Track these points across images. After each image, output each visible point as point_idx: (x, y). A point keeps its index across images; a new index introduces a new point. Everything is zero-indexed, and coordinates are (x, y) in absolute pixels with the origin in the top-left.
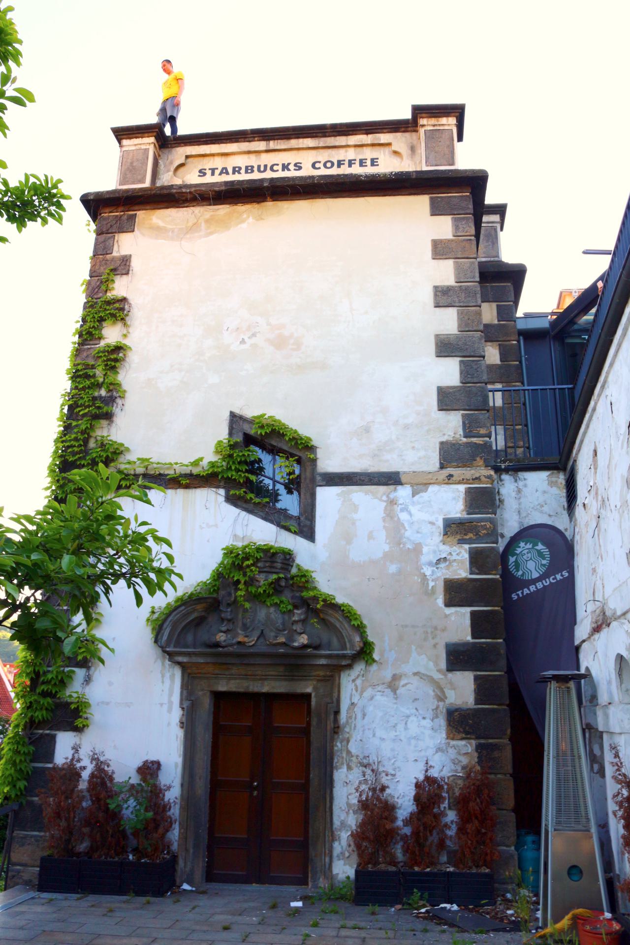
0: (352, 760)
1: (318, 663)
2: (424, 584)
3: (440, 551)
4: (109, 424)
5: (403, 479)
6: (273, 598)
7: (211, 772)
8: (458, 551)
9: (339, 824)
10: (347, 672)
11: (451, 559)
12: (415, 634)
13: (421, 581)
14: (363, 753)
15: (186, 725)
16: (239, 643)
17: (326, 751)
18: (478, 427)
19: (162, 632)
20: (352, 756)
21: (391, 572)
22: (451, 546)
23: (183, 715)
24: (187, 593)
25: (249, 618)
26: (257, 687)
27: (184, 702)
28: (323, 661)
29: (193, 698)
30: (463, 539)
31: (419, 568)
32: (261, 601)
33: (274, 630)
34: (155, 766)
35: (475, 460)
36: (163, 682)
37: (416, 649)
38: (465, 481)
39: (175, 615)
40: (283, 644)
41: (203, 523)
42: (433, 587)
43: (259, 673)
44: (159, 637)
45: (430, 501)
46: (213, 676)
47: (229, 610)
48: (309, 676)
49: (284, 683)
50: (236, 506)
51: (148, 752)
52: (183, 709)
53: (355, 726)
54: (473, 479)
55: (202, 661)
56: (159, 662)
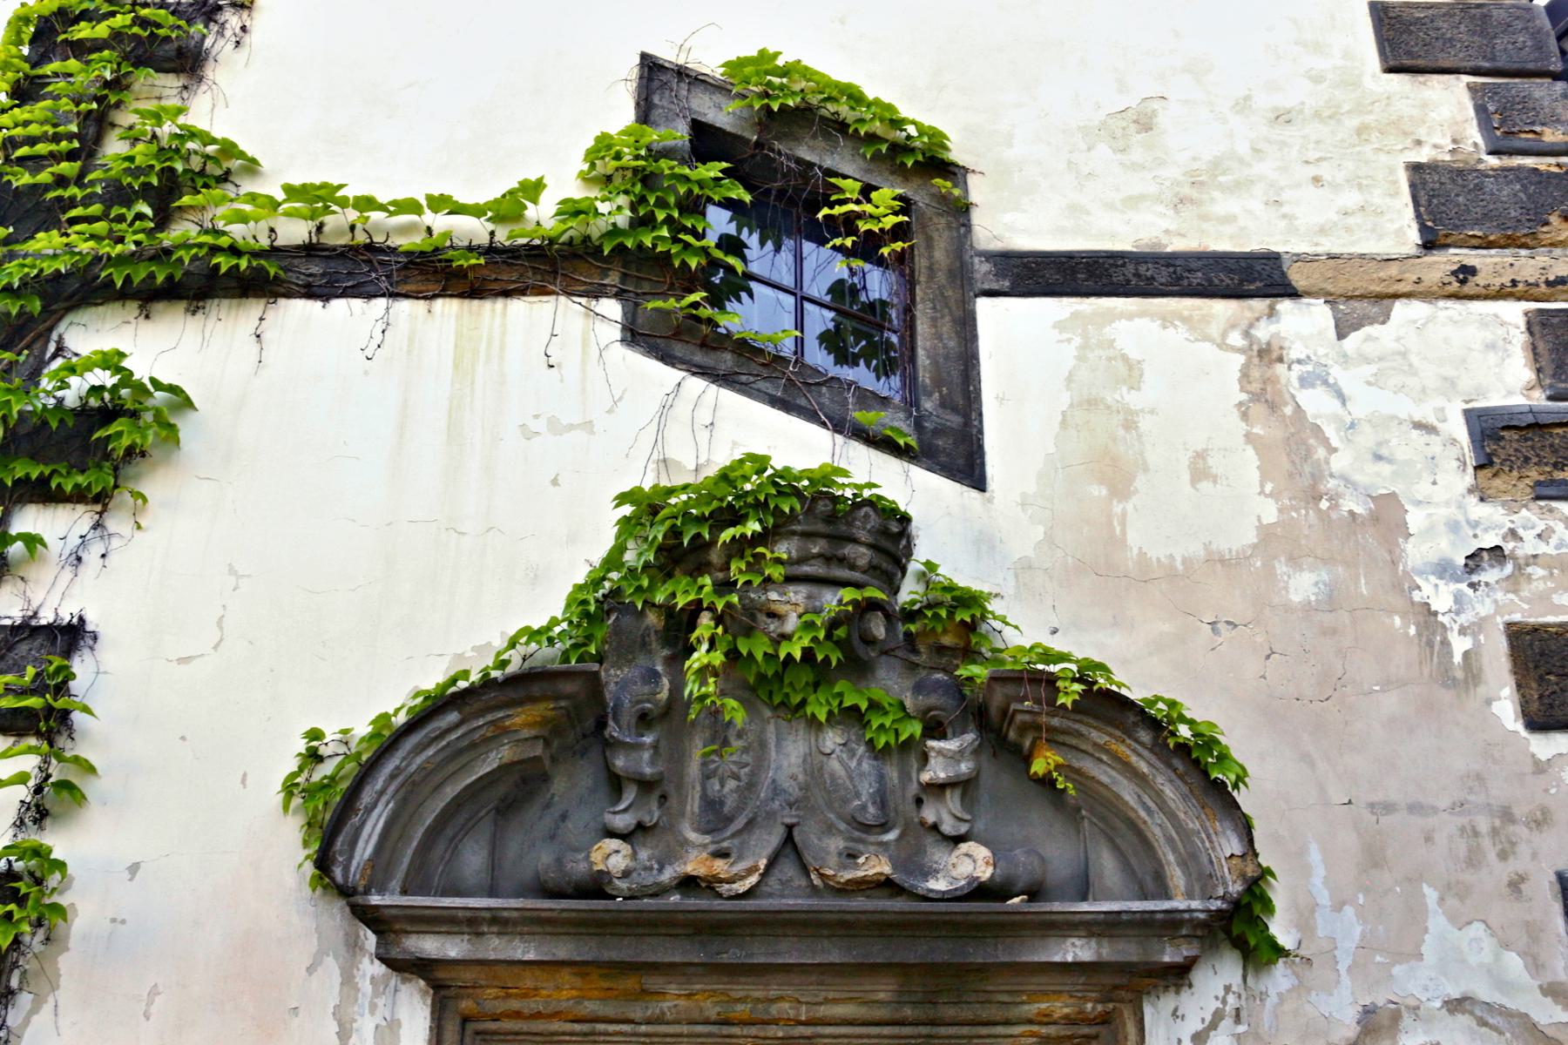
1: (1057, 959)
2: (1430, 644)
3: (1475, 525)
4: (185, 87)
5: (1297, 278)
6: (837, 689)
8: (1541, 526)
10: (1167, 1002)
11: (1519, 553)
12: (1428, 839)
13: (1419, 634)
16: (688, 883)
18: (1533, 123)
21: (1296, 598)
22: (1512, 507)
24: (465, 674)
25: (736, 777)
28: (1077, 950)
30: (1552, 482)
31: (1403, 585)
32: (783, 704)
33: (842, 826)
35: (1547, 223)
37: (1441, 900)
38: (1521, 287)
40: (886, 885)
41: (536, 417)
42: (1466, 655)
43: (784, 1009)
45: (1404, 355)
46: (577, 1027)
47: (648, 739)
48: (1007, 1023)
50: (667, 359)
54: (1548, 283)
55: (531, 956)
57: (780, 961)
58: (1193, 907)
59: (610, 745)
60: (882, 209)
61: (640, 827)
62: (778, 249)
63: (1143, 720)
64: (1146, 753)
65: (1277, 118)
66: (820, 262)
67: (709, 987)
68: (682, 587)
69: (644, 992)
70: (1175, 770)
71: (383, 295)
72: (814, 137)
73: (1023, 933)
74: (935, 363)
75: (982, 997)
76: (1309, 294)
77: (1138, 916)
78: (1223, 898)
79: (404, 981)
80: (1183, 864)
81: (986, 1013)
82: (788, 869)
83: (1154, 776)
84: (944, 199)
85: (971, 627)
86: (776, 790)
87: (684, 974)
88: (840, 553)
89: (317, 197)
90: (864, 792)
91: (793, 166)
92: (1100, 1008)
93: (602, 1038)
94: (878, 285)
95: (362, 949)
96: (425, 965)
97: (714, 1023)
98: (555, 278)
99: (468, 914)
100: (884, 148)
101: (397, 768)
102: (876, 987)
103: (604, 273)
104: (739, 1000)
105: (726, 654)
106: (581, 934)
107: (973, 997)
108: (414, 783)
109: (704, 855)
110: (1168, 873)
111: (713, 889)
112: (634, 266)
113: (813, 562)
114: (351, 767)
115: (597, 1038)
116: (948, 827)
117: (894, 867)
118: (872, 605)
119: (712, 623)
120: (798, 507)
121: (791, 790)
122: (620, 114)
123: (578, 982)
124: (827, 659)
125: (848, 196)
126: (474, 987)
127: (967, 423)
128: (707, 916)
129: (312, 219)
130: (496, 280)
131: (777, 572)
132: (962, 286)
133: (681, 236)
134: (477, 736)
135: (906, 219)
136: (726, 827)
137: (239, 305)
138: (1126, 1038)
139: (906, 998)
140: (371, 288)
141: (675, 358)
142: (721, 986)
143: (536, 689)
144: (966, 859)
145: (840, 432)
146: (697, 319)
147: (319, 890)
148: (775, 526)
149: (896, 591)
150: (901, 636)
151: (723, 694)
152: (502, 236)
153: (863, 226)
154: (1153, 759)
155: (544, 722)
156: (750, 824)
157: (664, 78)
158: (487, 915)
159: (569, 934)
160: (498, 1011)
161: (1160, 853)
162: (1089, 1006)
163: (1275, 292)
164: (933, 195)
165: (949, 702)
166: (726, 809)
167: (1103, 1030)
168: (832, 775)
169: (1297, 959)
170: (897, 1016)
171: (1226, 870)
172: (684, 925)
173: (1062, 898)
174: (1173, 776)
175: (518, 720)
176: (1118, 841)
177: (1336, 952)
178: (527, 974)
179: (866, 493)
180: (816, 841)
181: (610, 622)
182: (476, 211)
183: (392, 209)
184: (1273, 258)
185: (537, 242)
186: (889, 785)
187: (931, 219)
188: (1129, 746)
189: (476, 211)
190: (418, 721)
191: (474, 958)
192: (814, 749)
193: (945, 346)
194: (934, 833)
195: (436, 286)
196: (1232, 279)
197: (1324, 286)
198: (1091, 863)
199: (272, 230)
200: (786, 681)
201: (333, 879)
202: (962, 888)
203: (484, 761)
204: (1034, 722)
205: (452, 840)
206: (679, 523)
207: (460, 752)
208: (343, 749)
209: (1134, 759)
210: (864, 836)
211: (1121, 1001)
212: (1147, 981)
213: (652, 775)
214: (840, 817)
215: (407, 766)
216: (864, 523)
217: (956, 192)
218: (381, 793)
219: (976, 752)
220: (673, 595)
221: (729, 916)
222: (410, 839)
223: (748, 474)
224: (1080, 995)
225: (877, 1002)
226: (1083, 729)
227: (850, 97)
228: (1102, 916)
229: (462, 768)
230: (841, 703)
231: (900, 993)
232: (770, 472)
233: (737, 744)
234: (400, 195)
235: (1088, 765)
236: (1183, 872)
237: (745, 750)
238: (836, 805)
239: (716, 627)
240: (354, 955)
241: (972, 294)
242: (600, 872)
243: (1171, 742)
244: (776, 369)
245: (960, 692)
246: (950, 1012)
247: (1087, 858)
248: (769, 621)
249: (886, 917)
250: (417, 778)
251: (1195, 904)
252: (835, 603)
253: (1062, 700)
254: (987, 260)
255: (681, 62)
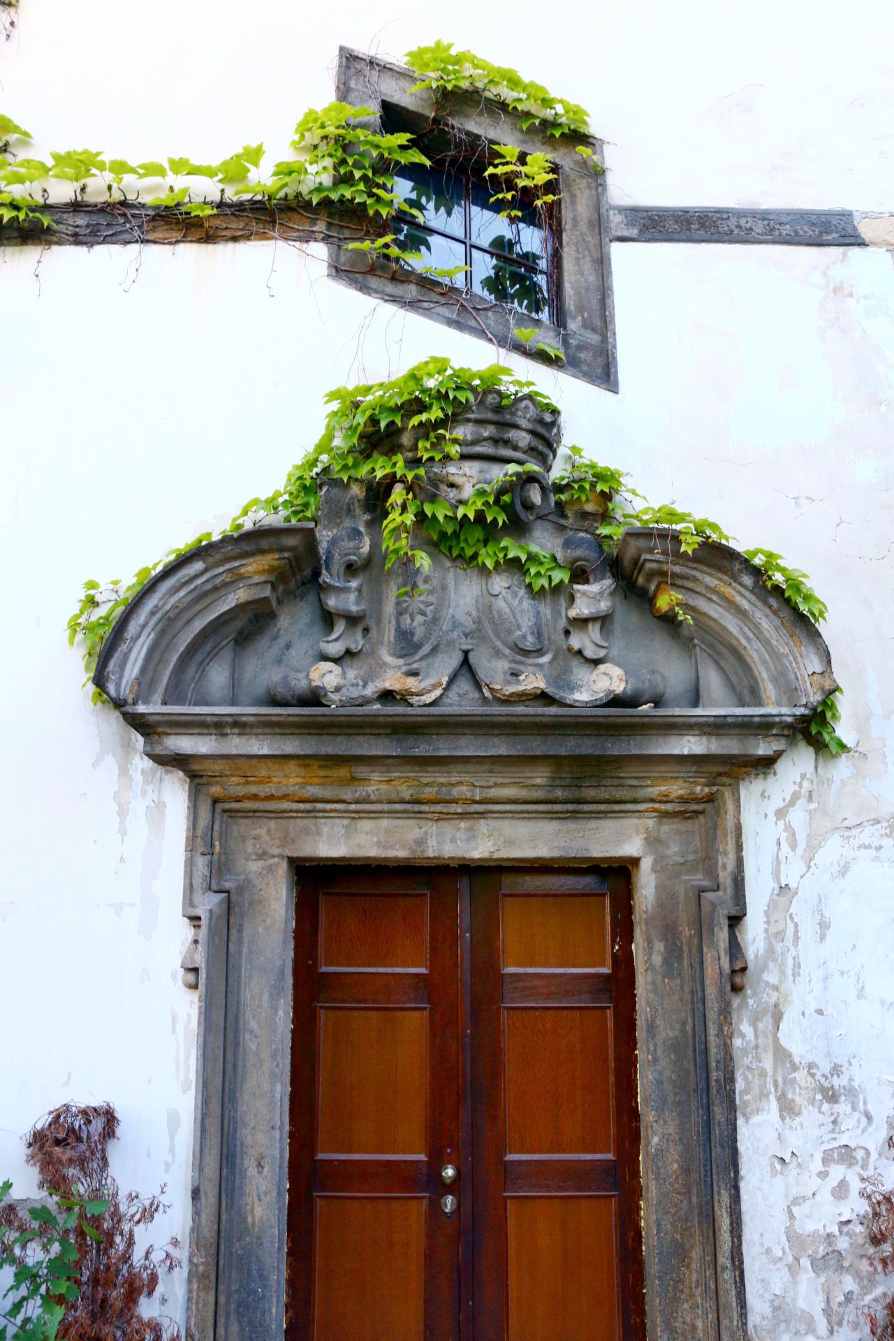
0: (794, 1081)
1: (676, 752)
5: (865, 231)
6: (503, 544)
7: (291, 1135)
9: (768, 1311)
14: (829, 1054)
15: (208, 977)
16: (387, 696)
17: (706, 1051)
19: (123, 647)
20: (795, 1068)
23: (196, 942)
25: (423, 613)
26: (453, 840)
27: (198, 897)
29: (227, 885)
32: (460, 556)
33: (507, 651)
34: (98, 1125)
36: (123, 831)
39: (176, 590)
40: (544, 697)
43: (463, 791)
44: (112, 665)
46: (302, 806)
47: (354, 584)
48: (635, 801)
49: (549, 828)
51: (69, 1074)
52: (195, 919)
53: (797, 966)
55: (265, 751)
56: (111, 763)
57: (460, 754)
58: (782, 712)
59: (324, 589)
60: (536, 171)
61: (348, 653)
62: (449, 213)
63: (746, 568)
64: (748, 594)
65: (852, 103)
66: (483, 221)
67: (404, 775)
68: (380, 463)
69: (353, 779)
70: (770, 607)
71: (137, 241)
72: (481, 114)
73: (650, 732)
74: (578, 293)
75: (616, 782)
76: (874, 244)
77: (740, 719)
78: (806, 706)
79: (167, 772)
80: (775, 680)
81: (619, 794)
82: (464, 685)
83: (753, 612)
84: (584, 164)
85: (606, 497)
86: (455, 624)
87: (386, 765)
88: (506, 436)
89: (80, 164)
90: (525, 625)
91: (464, 137)
92: (706, 790)
93: (321, 814)
94: (531, 240)
95: (134, 749)
96: (182, 760)
97: (408, 802)
98: (274, 227)
99: (215, 719)
100: (537, 122)
101: (156, 606)
102: (535, 775)
103: (314, 222)
104: (427, 785)
105: (416, 515)
106: (303, 734)
107: (609, 782)
108: (169, 619)
109: (399, 674)
110: (762, 688)
111: (406, 700)
112: (337, 216)
113: (484, 443)
114: (120, 609)
115: (317, 815)
116: (590, 652)
117: (548, 683)
118: (531, 479)
119: (404, 492)
120: (472, 398)
121: (466, 624)
122: (323, 95)
123: (302, 772)
124: (495, 520)
125: (508, 159)
126: (221, 776)
127: (605, 340)
128: (403, 719)
129: (77, 180)
130: (226, 228)
131: (454, 450)
132: (600, 233)
133: (375, 190)
134: (218, 581)
135: (555, 176)
136: (415, 652)
137: (21, 251)
138: (726, 812)
139: (558, 782)
140: (126, 237)
141: (371, 289)
142: (413, 774)
143: (264, 544)
144: (604, 677)
145: (503, 347)
146: (387, 257)
147: (99, 704)
148: (454, 414)
149: (549, 469)
150: (553, 504)
151: (412, 548)
152: (231, 195)
153: (521, 183)
154: (753, 598)
155: (271, 570)
156: (435, 650)
157: (358, 67)
158: (229, 719)
159: (294, 734)
160: (241, 795)
161: (756, 672)
162: (698, 789)
163: (848, 241)
164: (576, 162)
165: (592, 555)
166: (416, 639)
167: (708, 807)
168: (499, 612)
169: (857, 754)
170: (551, 796)
171: (808, 684)
172: (384, 726)
173: (678, 706)
174: (768, 611)
175: (250, 568)
176: (722, 663)
177: (885, 750)
178: (263, 765)
179: (526, 390)
180: (486, 662)
181: (322, 493)
182: (209, 172)
183: (141, 171)
184: (846, 216)
185: (259, 197)
186: (544, 621)
187: (574, 180)
188: (734, 589)
189: (209, 172)
190: (170, 571)
191: (220, 753)
192: (485, 592)
193: (586, 280)
194: (579, 657)
195: (178, 234)
196: (813, 231)
197: (886, 237)
198: (701, 683)
199: (45, 191)
200: (462, 538)
201: (108, 694)
202: (601, 699)
203: (225, 601)
204: (660, 569)
205: (201, 663)
206: (377, 412)
207: (205, 594)
208: (114, 596)
209: (738, 599)
210: (523, 659)
211: (723, 785)
212: (744, 769)
213: (358, 612)
214: (504, 643)
215: (163, 605)
216: (524, 413)
217: (595, 158)
218: (144, 626)
219: (612, 594)
220: (373, 470)
221: (419, 719)
222: (168, 662)
223: (432, 373)
224: (691, 780)
225: (534, 785)
226: (698, 575)
227: (510, 80)
228: (712, 719)
229: (204, 608)
230: (506, 555)
231: (553, 778)
232: (449, 372)
233: (422, 587)
234: (147, 160)
235: (701, 604)
236: (774, 687)
237: (431, 592)
238: (502, 635)
239: (407, 494)
240: (128, 753)
241: (607, 239)
242: (318, 687)
243: (769, 584)
244: (451, 298)
245: (600, 546)
246: (591, 793)
247: (697, 677)
248: (449, 490)
249: (544, 719)
250: (171, 615)
251: (785, 710)
252: (501, 476)
253: (683, 549)
254: (620, 213)
255: (372, 53)
